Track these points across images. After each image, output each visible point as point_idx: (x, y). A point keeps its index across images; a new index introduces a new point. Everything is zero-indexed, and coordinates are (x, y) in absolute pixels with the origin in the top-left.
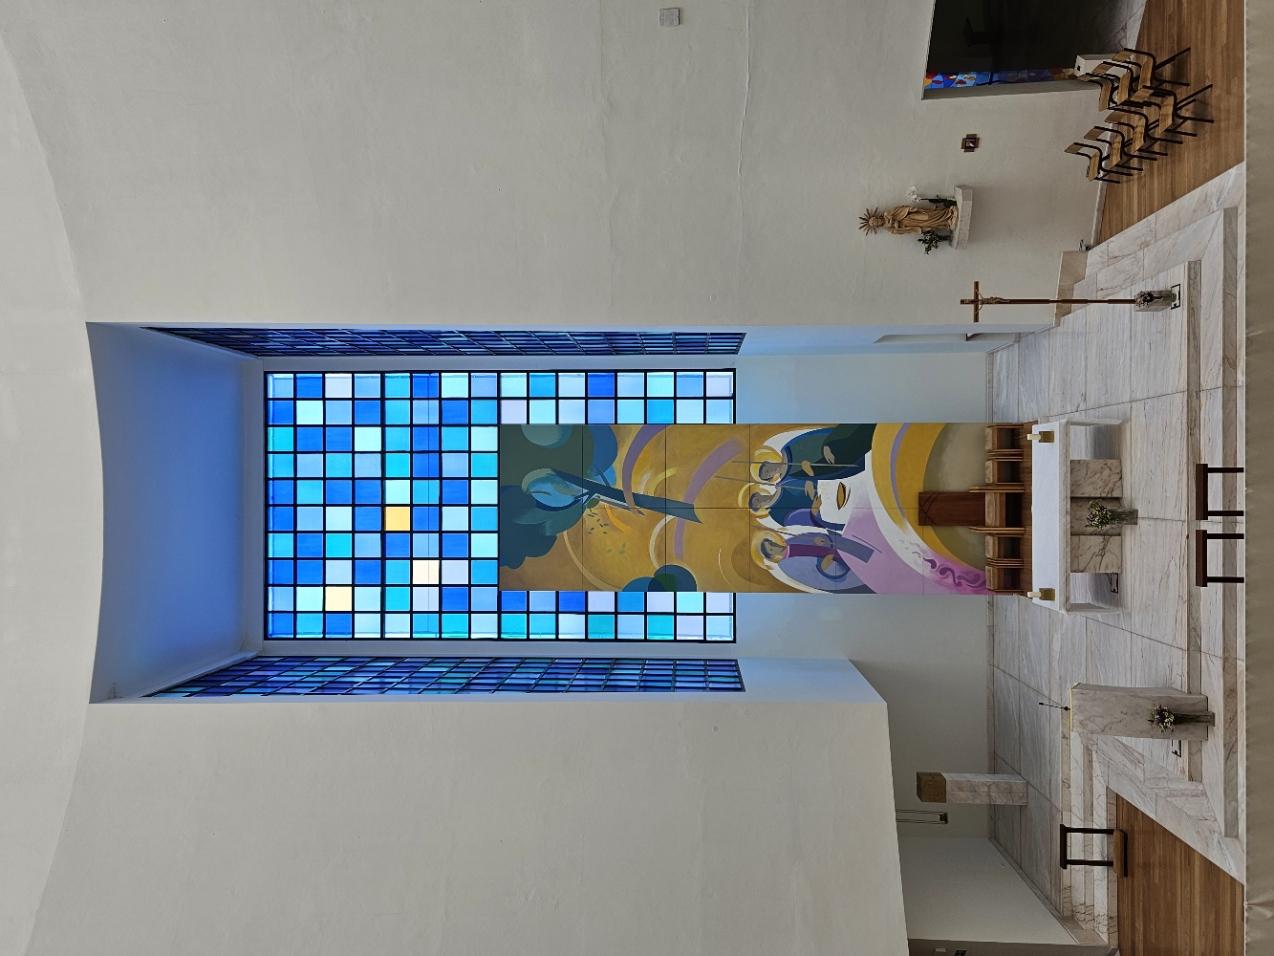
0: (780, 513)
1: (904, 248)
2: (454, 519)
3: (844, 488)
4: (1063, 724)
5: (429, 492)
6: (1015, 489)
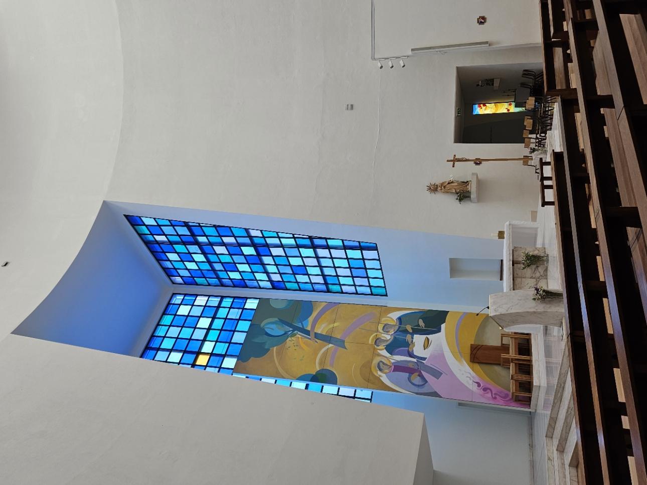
0: (391, 348)
1: (449, 201)
3: (428, 339)
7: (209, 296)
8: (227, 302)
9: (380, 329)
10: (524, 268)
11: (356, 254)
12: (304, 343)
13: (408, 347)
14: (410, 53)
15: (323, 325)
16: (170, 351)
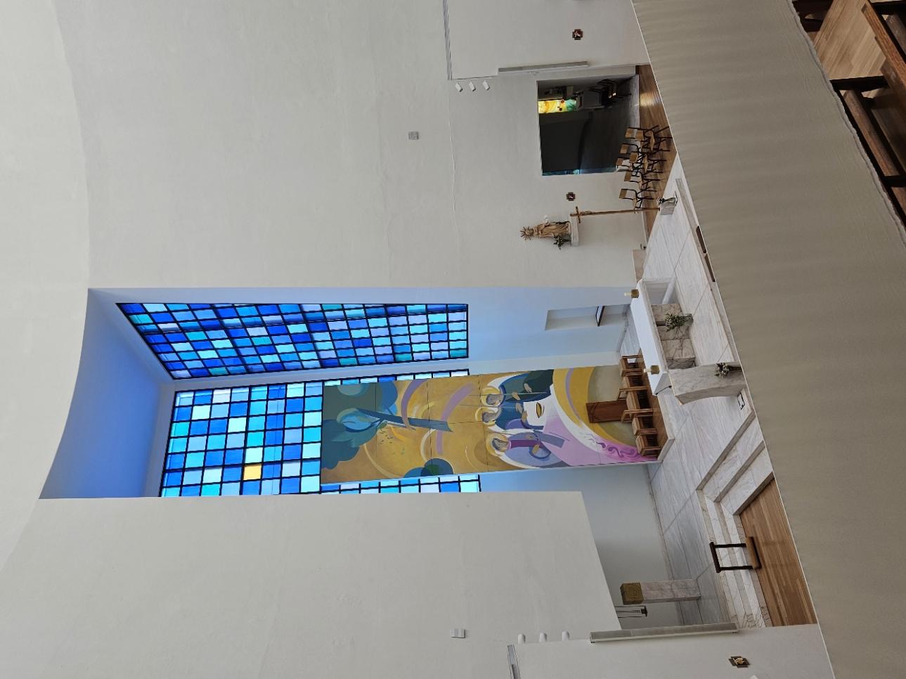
0: (502, 422)
1: (545, 247)
2: (291, 469)
3: (540, 405)
4: (701, 502)
5: (274, 454)
6: (640, 388)
7: (232, 388)
8: (260, 393)
9: (484, 402)
10: (668, 330)
11: (442, 317)
12: (399, 433)
13: (521, 417)
14: (496, 73)
15: (416, 408)
16: (203, 469)
